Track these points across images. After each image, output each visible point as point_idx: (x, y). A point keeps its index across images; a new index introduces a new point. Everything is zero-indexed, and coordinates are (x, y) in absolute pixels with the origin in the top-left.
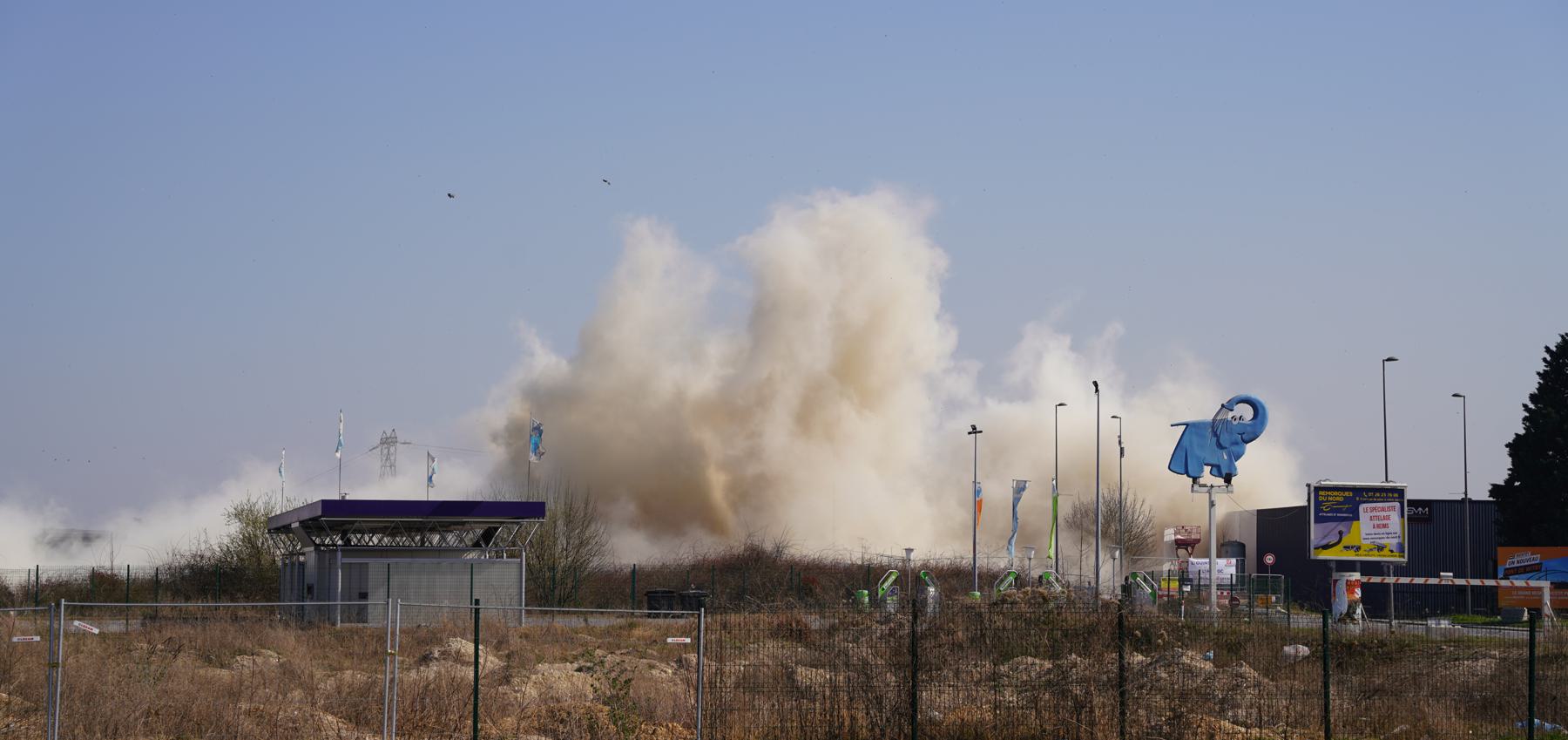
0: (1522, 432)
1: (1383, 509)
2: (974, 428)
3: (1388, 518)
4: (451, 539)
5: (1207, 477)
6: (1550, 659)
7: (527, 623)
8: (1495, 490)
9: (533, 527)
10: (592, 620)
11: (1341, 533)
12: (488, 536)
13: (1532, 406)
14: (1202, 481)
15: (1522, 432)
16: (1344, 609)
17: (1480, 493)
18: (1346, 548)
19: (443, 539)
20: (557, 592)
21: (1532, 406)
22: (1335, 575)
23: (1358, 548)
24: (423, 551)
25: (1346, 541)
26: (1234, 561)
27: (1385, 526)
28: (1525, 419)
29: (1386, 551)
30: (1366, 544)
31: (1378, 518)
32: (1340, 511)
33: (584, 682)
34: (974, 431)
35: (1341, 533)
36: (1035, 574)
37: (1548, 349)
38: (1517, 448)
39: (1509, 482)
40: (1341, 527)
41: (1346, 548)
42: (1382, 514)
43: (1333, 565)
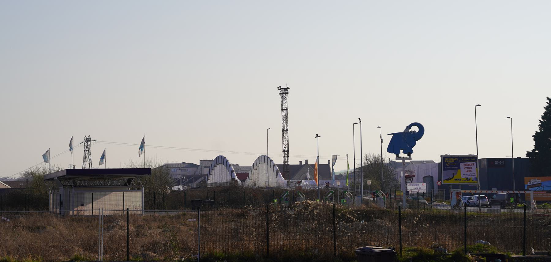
0: (539, 131)
1: (469, 165)
2: (317, 135)
4: (115, 182)
5: (402, 155)
6: (132, 215)
7: (145, 214)
8: (528, 154)
9: (147, 177)
10: (170, 213)
11: (453, 174)
12: (129, 181)
13: (542, 120)
14: (400, 155)
15: (539, 131)
17: (524, 156)
18: (456, 180)
19: (112, 182)
20: (156, 201)
21: (542, 120)
22: (452, 190)
23: (460, 180)
24: (105, 186)
25: (456, 177)
27: (470, 171)
28: (539, 125)
29: (471, 181)
30: (463, 178)
31: (467, 168)
33: (87, 210)
34: (317, 136)
35: (453, 174)
37: (306, 161)
38: (537, 137)
39: (534, 151)
41: (456, 180)
42: (469, 167)
43: (451, 187)
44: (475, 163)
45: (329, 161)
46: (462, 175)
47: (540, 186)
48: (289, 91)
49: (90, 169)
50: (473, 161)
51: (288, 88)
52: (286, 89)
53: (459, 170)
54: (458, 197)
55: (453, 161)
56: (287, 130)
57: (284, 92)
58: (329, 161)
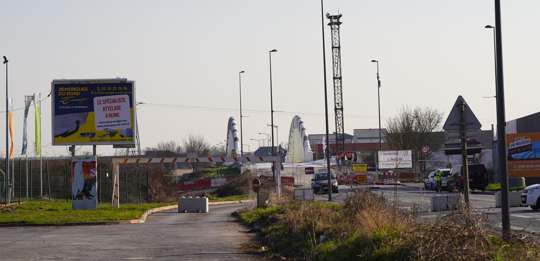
1: (114, 101)
3: (118, 108)
11: (78, 123)
16: (81, 187)
18: (83, 135)
25: (83, 128)
26: (410, 152)
27: (116, 115)
29: (117, 136)
31: (110, 108)
32: (77, 104)
35: (78, 123)
36: (285, 165)
40: (75, 117)
41: (83, 135)
42: (114, 105)
44: (127, 97)
45: (492, 125)
46: (97, 124)
47: (530, 150)
48: (341, 20)
49: (268, 147)
50: (123, 92)
51: (340, 16)
52: (335, 17)
53: (90, 113)
54: (89, 172)
55: (78, 94)
56: (340, 78)
57: (335, 21)
58: (492, 125)
